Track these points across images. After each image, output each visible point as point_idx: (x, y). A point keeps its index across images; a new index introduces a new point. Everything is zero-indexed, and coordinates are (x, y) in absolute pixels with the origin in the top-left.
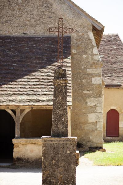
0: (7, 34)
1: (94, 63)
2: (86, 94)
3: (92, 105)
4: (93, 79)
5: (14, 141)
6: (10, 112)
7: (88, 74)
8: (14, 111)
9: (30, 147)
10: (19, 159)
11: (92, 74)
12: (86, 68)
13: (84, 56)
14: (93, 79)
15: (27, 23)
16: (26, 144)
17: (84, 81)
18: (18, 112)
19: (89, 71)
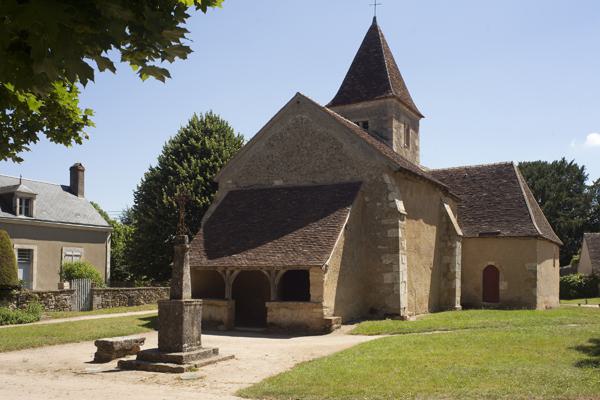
0: (295, 183)
1: (389, 212)
2: (380, 250)
3: (389, 262)
4: (389, 232)
5: (267, 304)
6: (265, 273)
7: (384, 226)
8: (269, 272)
9: (282, 311)
10: (272, 324)
11: (386, 225)
12: (380, 219)
13: (378, 204)
14: (389, 232)
15: (317, 169)
16: (279, 308)
17: (378, 234)
18: (273, 272)
19: (385, 222)
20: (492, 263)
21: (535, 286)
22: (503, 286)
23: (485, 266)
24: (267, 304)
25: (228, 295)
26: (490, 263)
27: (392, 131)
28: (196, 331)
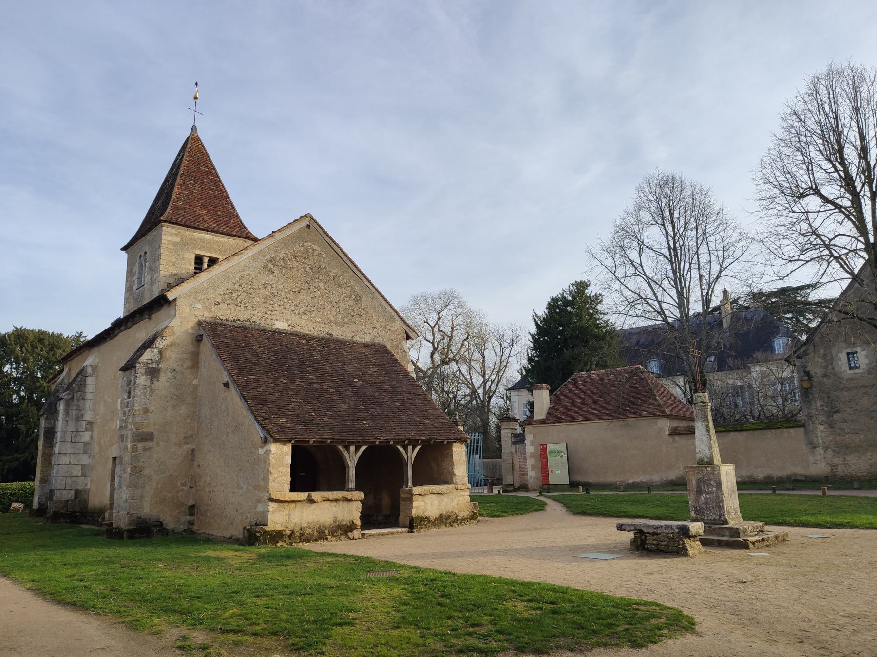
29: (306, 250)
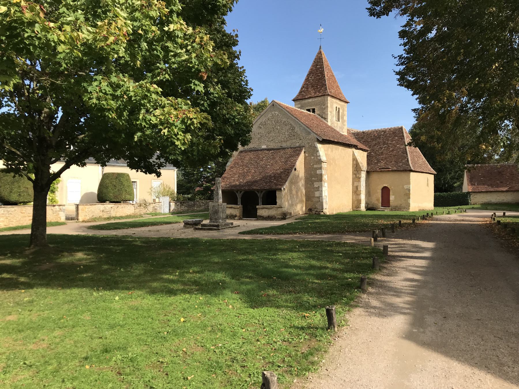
3: (317, 186)
12: (313, 165)
13: (312, 157)
19: (315, 166)
20: (386, 185)
21: (409, 198)
22: (392, 198)
23: (382, 187)
24: (257, 207)
25: (239, 200)
26: (385, 185)
27: (327, 114)
28: (239, 107)
29: (273, 115)
